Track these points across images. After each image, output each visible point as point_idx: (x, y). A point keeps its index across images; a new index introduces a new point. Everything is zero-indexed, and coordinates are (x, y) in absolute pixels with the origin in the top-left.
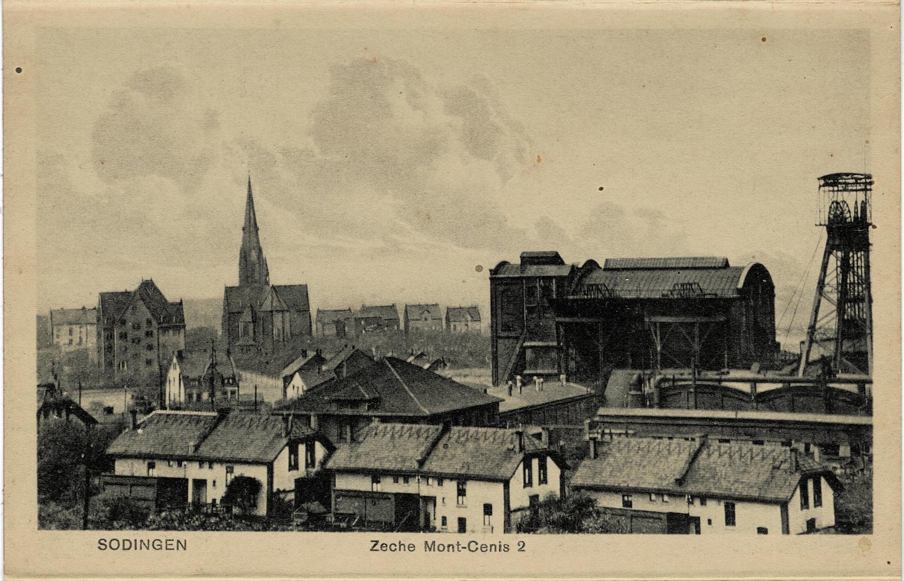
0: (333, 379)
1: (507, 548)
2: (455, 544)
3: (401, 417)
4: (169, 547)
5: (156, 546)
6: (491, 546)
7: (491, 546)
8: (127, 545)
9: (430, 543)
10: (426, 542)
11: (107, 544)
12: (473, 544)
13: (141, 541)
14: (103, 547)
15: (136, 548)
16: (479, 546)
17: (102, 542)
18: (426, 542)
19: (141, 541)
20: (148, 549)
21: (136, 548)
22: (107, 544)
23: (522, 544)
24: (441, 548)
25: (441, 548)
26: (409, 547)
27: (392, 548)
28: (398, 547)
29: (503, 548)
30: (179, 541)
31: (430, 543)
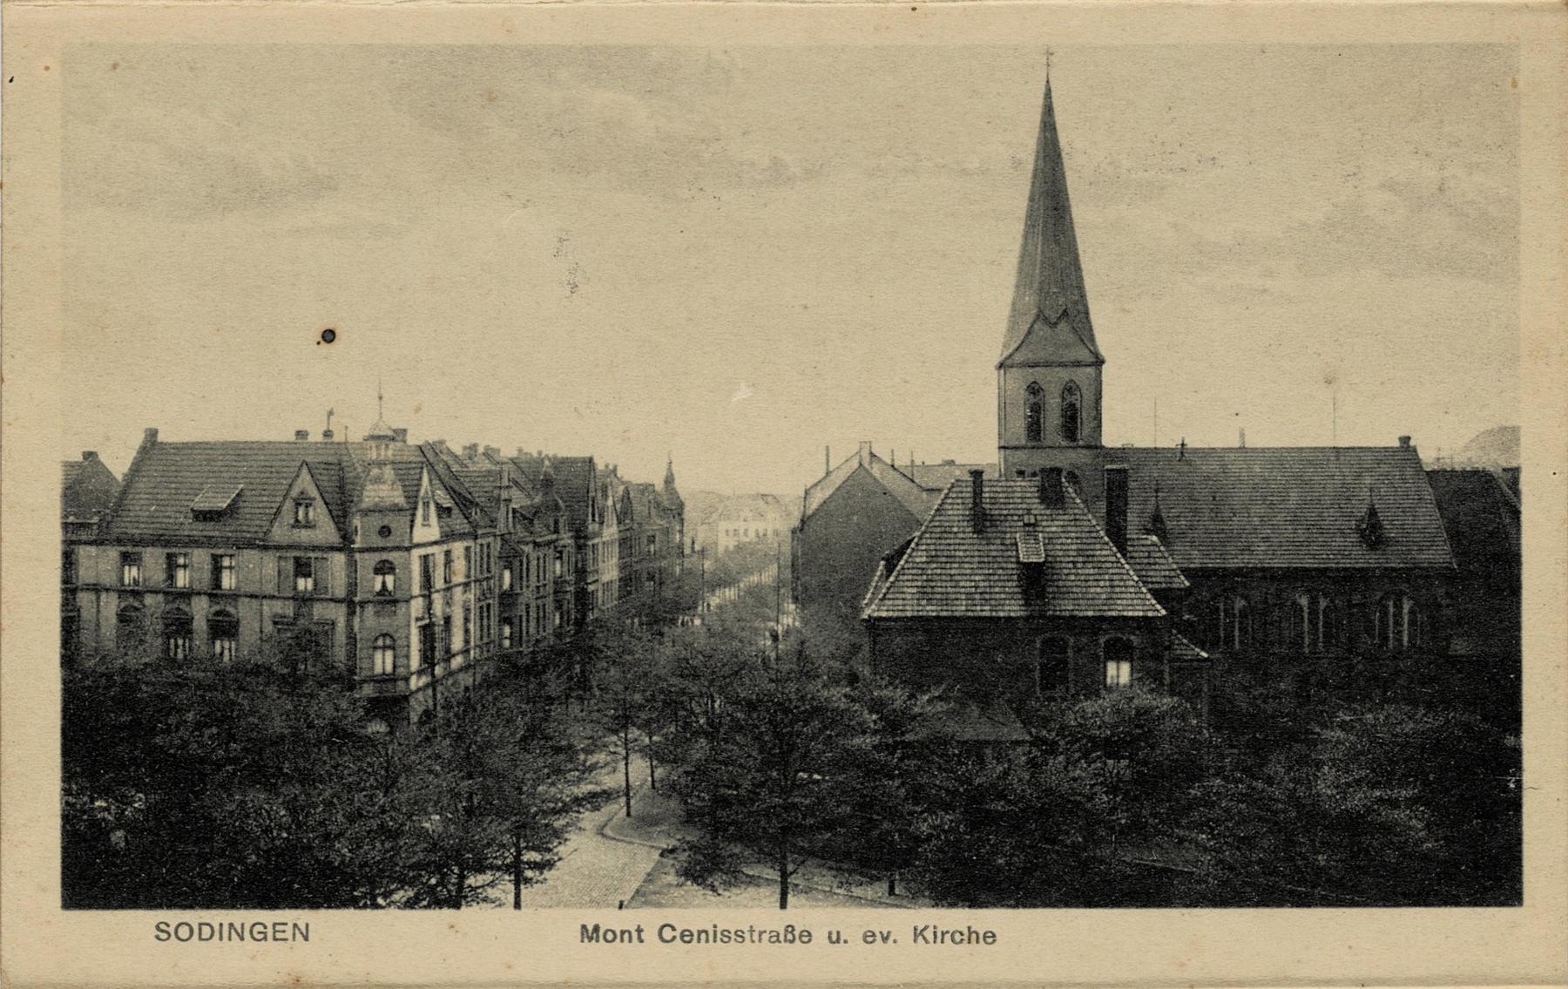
0: (467, 549)
1: (807, 936)
2: (746, 929)
3: (433, 649)
4: (279, 935)
5: (260, 935)
6: (700, 933)
7: (700, 933)
8: (206, 931)
9: (590, 928)
10: (584, 927)
11: (171, 930)
12: (186, 928)
13: (231, 925)
14: (164, 936)
15: (221, 938)
16: (677, 933)
17: (163, 927)
18: (584, 927)
19: (231, 925)
20: (242, 939)
21: (221, 938)
22: (171, 930)
23: (667, 933)
24: (610, 936)
25: (610, 936)
26: (682, 936)
27: (215, 933)
28: (965, 937)
29: (747, 935)
30: (295, 925)
31: (590, 928)
